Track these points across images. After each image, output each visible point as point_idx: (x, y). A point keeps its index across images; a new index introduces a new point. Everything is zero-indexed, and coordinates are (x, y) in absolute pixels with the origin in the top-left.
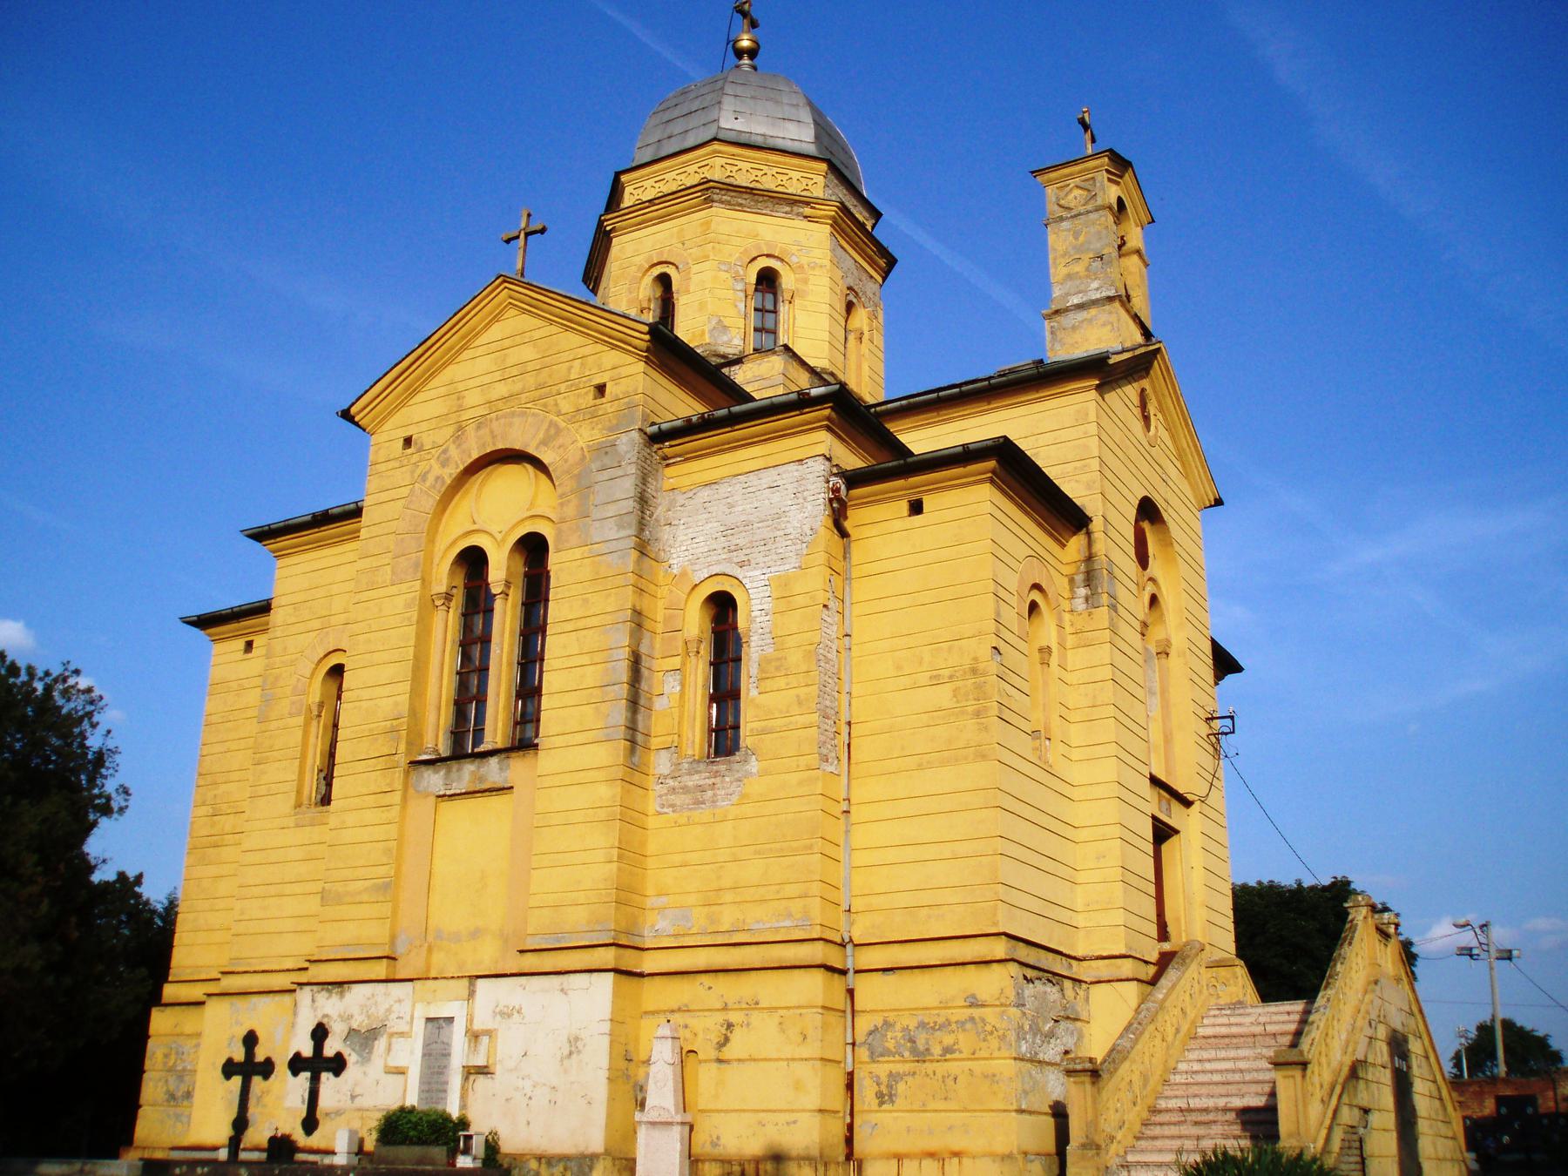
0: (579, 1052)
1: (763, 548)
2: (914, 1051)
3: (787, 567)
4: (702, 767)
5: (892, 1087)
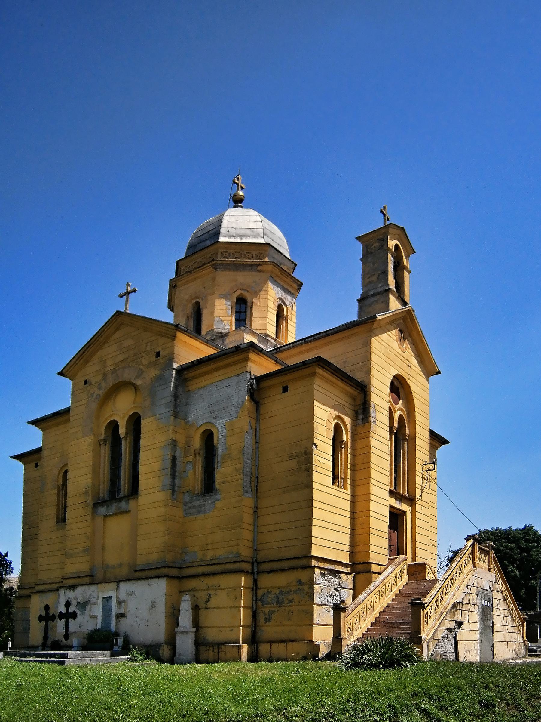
1: (224, 411)
2: (278, 602)
3: (232, 418)
4: (200, 498)
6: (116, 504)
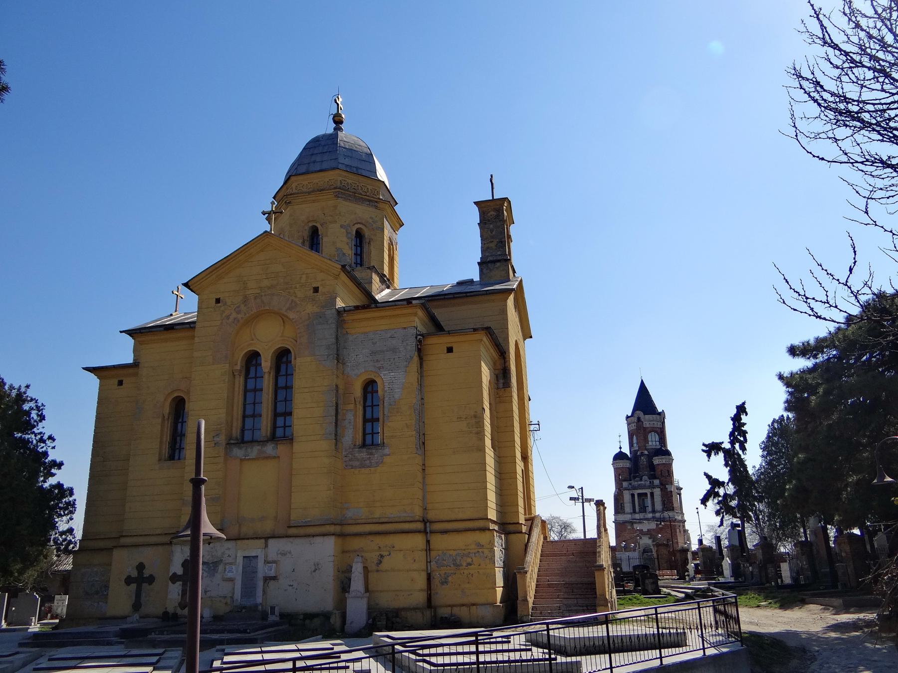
0: (319, 569)
5: (446, 579)
6: (259, 447)
